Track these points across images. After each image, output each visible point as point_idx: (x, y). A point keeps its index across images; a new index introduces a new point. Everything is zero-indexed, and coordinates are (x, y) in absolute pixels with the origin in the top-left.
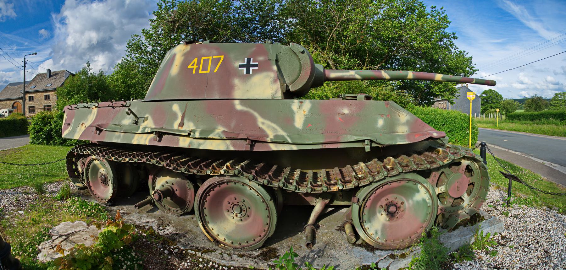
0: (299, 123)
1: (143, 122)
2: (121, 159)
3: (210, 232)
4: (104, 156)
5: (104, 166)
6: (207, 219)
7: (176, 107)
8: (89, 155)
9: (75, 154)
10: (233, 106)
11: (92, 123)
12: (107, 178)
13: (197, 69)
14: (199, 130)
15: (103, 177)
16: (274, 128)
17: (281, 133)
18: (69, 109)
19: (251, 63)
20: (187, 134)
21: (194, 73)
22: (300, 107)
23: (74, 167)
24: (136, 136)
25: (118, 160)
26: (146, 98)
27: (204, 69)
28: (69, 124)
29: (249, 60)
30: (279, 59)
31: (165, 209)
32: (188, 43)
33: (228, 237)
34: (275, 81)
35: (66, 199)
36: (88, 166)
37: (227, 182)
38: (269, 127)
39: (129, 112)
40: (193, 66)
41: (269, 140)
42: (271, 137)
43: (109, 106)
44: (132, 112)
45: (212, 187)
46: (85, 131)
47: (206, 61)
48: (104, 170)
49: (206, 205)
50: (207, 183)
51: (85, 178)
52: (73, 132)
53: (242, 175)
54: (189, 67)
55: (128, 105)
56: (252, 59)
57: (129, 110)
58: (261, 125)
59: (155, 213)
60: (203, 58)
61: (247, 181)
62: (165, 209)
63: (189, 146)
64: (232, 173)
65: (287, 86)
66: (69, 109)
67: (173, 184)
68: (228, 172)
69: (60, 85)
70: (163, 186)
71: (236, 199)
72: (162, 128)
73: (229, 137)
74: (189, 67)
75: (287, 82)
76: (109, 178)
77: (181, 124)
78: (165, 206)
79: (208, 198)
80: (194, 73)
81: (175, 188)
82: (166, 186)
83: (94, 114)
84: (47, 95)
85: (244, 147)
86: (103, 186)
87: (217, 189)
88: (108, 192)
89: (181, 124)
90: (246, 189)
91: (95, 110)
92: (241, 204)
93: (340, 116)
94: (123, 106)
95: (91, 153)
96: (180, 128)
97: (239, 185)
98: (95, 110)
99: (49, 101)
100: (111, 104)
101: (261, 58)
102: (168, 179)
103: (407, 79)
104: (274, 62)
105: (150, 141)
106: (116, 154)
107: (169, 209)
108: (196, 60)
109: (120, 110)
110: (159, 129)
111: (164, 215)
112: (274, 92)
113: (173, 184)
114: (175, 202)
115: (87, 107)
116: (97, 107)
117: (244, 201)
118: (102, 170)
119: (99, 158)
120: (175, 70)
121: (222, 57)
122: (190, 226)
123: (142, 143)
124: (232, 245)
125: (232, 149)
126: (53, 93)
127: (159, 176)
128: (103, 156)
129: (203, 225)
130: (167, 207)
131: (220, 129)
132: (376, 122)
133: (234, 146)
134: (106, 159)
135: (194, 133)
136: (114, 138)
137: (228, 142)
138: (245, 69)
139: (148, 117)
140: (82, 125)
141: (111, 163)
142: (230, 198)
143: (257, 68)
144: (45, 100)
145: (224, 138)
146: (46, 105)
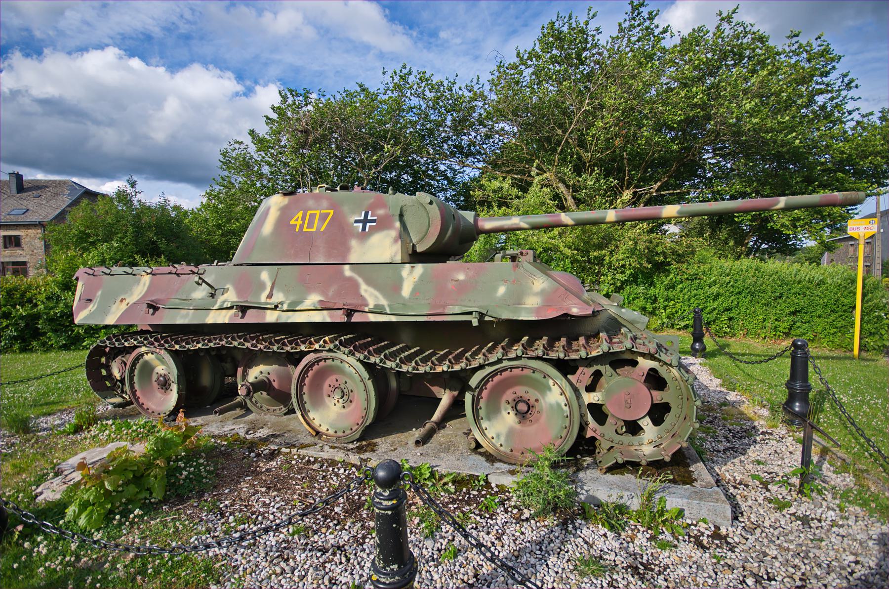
0: (406, 290)
1: (223, 294)
2: (189, 346)
3: (310, 422)
4: (163, 346)
5: (162, 361)
6: (307, 406)
7: (265, 275)
8: (135, 347)
9: (107, 350)
10: (342, 272)
11: (141, 298)
12: (169, 379)
13: (302, 226)
14: (288, 302)
15: (162, 379)
16: (376, 297)
17: (383, 302)
18: (89, 274)
19: (369, 218)
20: (273, 306)
21: (297, 230)
22: (411, 272)
23: (104, 372)
24: (212, 313)
25: (185, 347)
26: (236, 260)
27: (310, 225)
28: (90, 300)
29: (366, 214)
30: (404, 213)
31: (263, 410)
32: (285, 194)
33: (331, 425)
34: (395, 241)
35: (87, 428)
36: (134, 364)
37: (325, 359)
38: (371, 295)
39: (200, 281)
40: (296, 221)
41: (366, 309)
42: (372, 305)
43: (170, 273)
44: (204, 281)
45: (310, 366)
46: (126, 311)
47: (313, 216)
48: (164, 367)
49: (305, 389)
50: (304, 361)
51: (127, 388)
52: (104, 310)
53: (339, 349)
54: (292, 222)
55: (201, 271)
56: (370, 213)
57: (200, 278)
58: (363, 293)
59: (246, 418)
60: (309, 212)
61: (344, 357)
62: (263, 410)
63: (277, 320)
64: (327, 347)
65: (413, 244)
66: (89, 274)
67: (269, 374)
68: (324, 347)
69: (51, 217)
70: (256, 378)
71: (337, 381)
72: (247, 302)
73: (324, 306)
74: (292, 222)
75: (414, 241)
76: (172, 379)
77: (270, 296)
78: (261, 407)
79: (307, 381)
80: (297, 230)
81: (271, 378)
82: (261, 377)
83: (144, 284)
84: (10, 237)
85: (339, 317)
86: (162, 394)
87: (315, 367)
88: (172, 398)
89: (270, 296)
90: (345, 367)
91: (147, 279)
92: (342, 386)
93: (454, 283)
94: (194, 273)
95: (138, 343)
96: (268, 301)
97: (337, 362)
98: (147, 279)
99: (21, 252)
100: (174, 270)
101: (381, 212)
102: (262, 368)
103: (662, 219)
104: (397, 218)
105: (230, 318)
106: (183, 341)
107: (268, 410)
108: (300, 214)
109: (188, 278)
110: (241, 302)
111: (258, 417)
112: (393, 254)
113: (269, 374)
114: (273, 397)
115: (131, 274)
116: (151, 273)
117: (346, 383)
118: (160, 369)
119: (154, 350)
120: (268, 228)
121: (332, 212)
122: (292, 425)
123: (220, 321)
124: (335, 434)
125: (328, 320)
126: (31, 232)
127: (250, 367)
128: (161, 345)
129: (302, 415)
130: (265, 407)
131: (313, 299)
132: (495, 289)
133: (331, 317)
134: (166, 349)
135: (282, 305)
136: (178, 318)
137: (325, 312)
138: (361, 225)
139: (228, 289)
140: (122, 301)
141: (175, 354)
142: (330, 380)
143: (374, 224)
144: (5, 247)
145: (319, 308)
146: (7, 260)
